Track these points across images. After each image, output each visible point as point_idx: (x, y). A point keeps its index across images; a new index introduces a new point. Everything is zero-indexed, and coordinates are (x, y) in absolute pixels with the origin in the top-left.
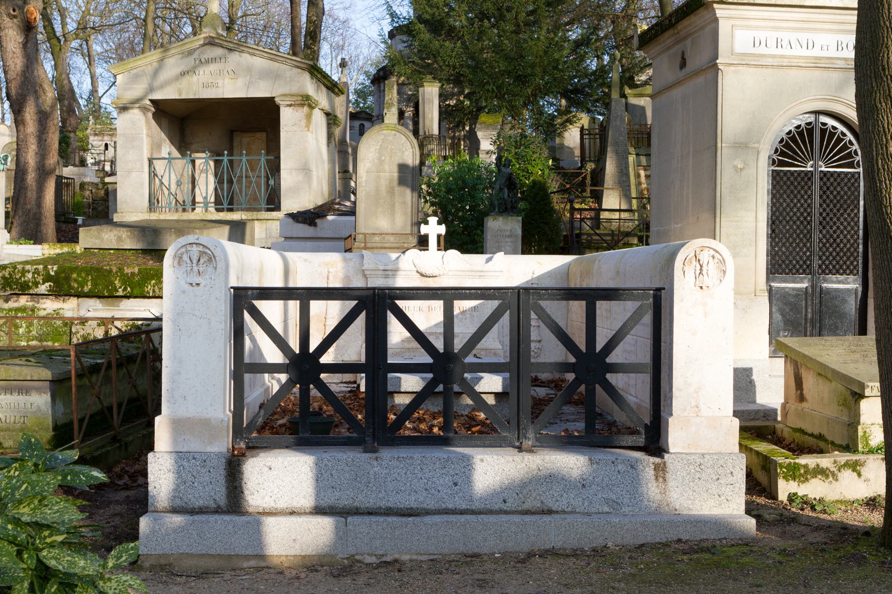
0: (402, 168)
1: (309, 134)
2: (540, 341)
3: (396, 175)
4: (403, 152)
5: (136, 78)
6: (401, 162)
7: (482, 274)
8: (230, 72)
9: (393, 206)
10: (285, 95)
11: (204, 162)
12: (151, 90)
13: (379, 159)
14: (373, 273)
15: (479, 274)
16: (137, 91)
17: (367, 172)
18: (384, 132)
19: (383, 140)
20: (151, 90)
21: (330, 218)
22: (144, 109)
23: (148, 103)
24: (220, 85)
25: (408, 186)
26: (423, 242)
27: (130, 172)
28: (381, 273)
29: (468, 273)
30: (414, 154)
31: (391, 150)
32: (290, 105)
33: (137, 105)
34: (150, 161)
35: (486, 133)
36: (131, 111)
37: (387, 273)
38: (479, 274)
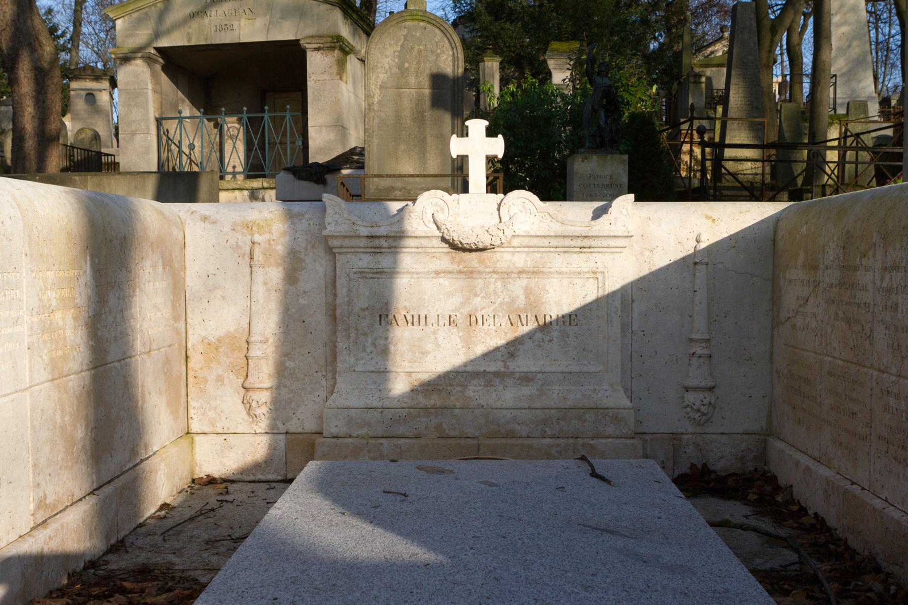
0: (437, 80)
1: (343, 85)
2: (711, 389)
3: (427, 92)
4: (438, 56)
5: (138, 23)
6: (434, 70)
7: (587, 243)
8: (247, 11)
9: (422, 141)
10: (312, 37)
11: (232, 125)
12: (157, 35)
13: (400, 67)
14: (347, 242)
15: (579, 243)
16: (142, 36)
17: (381, 88)
18: (407, 23)
19: (405, 36)
20: (157, 35)
21: (345, 172)
22: (149, 60)
23: (153, 51)
24: (235, 27)
25: (446, 110)
26: (456, 178)
27: (133, 134)
28: (363, 242)
29: (554, 242)
30: (455, 59)
31: (419, 52)
32: (318, 49)
33: (140, 55)
34: (159, 121)
35: (559, 62)
36: (133, 62)
37: (376, 242)
38: (579, 243)
